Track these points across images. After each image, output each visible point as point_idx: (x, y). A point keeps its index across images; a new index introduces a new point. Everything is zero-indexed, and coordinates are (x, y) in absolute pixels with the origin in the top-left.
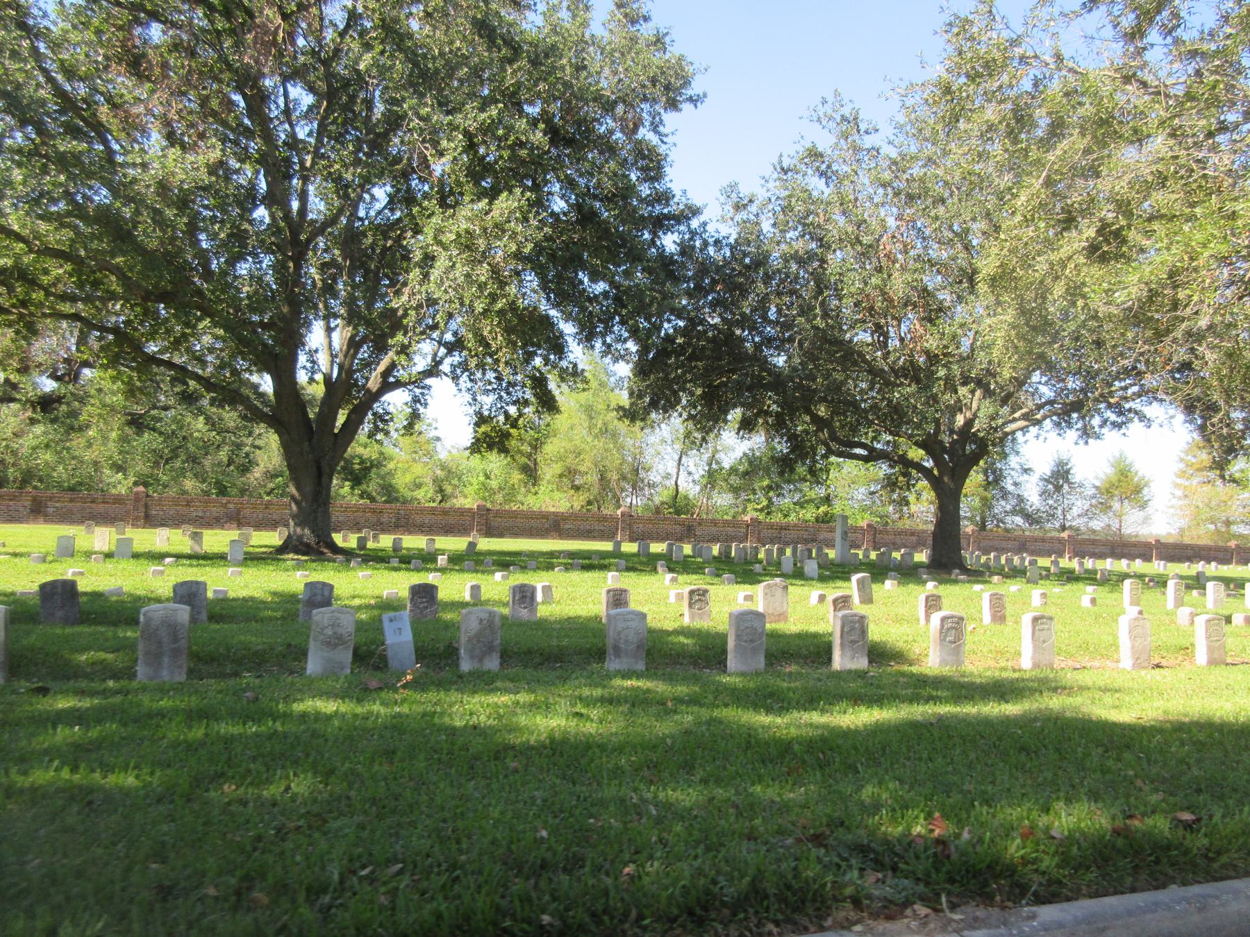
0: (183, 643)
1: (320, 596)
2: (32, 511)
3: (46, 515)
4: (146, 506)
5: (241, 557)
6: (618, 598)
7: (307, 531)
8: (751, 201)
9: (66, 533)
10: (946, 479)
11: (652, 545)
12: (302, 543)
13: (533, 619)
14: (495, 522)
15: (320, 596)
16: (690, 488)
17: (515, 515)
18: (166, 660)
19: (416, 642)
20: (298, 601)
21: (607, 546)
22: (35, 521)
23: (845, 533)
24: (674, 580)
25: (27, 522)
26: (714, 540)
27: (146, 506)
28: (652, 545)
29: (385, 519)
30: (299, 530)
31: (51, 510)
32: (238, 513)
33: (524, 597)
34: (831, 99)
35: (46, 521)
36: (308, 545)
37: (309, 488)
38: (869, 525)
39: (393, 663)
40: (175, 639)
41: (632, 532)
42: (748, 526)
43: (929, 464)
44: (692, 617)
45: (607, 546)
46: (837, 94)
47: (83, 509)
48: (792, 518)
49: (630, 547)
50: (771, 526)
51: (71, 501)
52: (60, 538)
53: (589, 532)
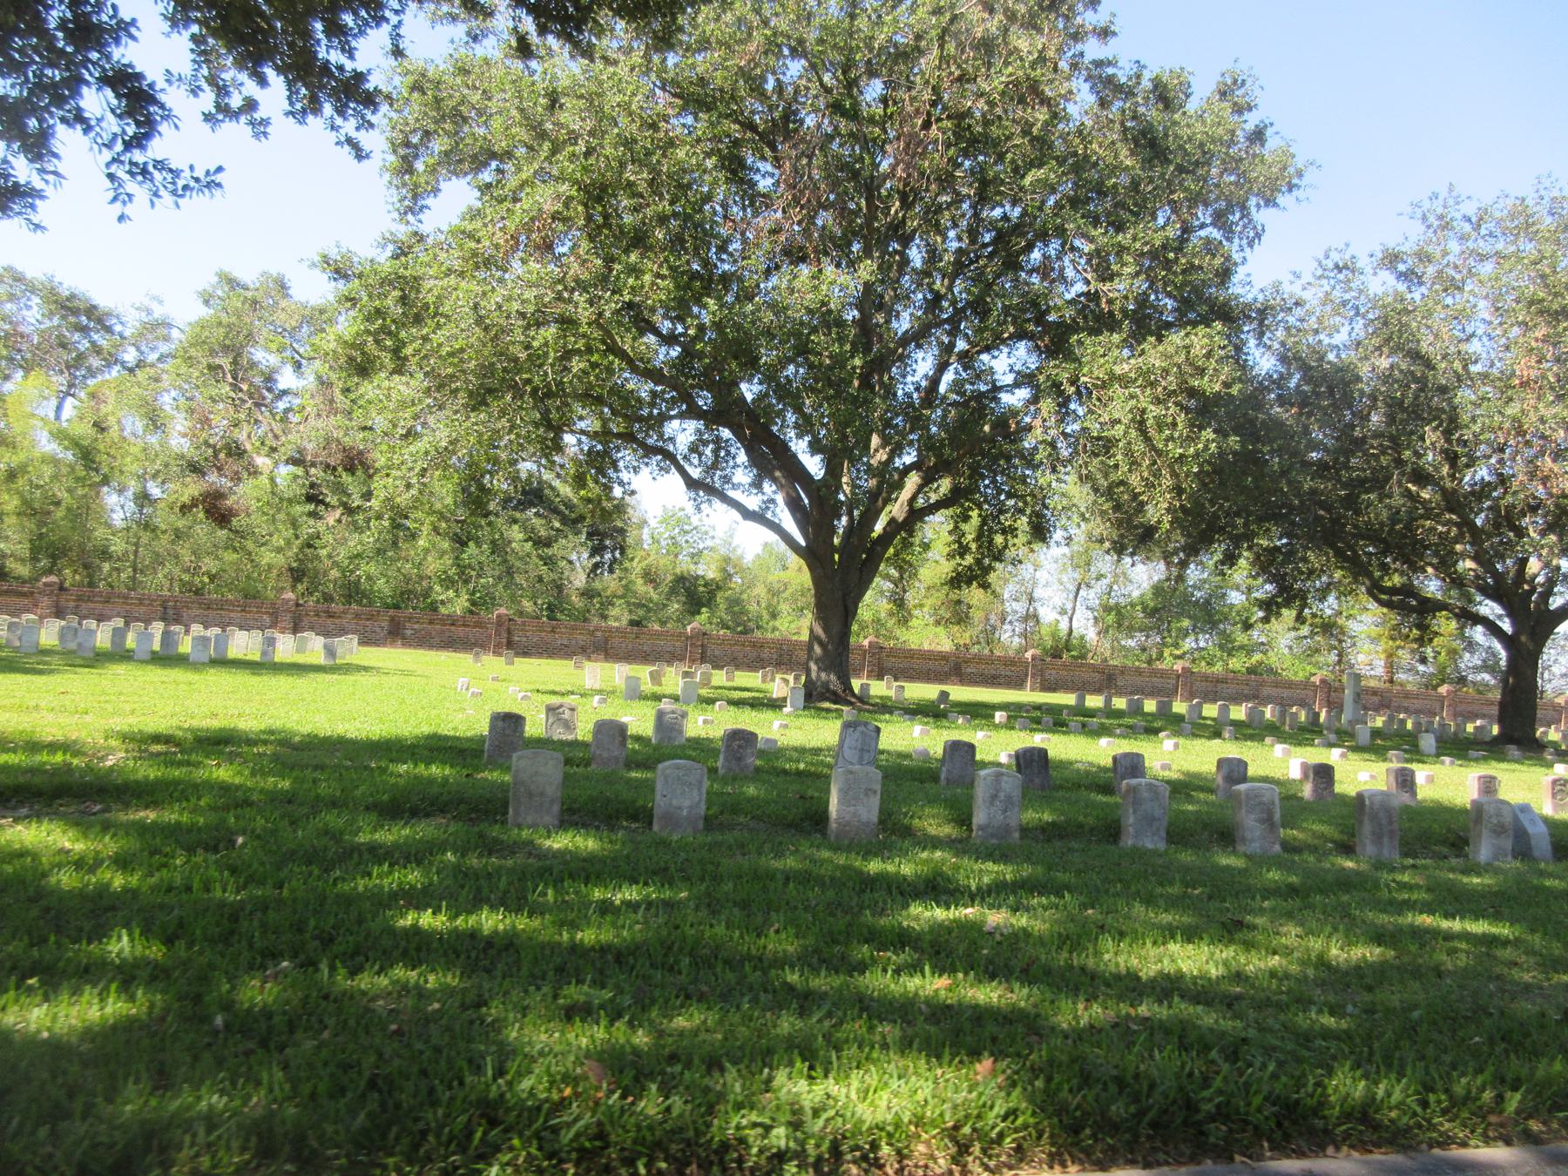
0: (1396, 826)
1: (1131, 765)
2: (390, 633)
3: (404, 638)
4: (509, 632)
5: (148, 657)
6: (1488, 785)
7: (833, 677)
8: (1297, 304)
9: (632, 674)
10: (1523, 638)
11: (1088, 697)
12: (828, 690)
13: (1413, 804)
14: (890, 662)
15: (1131, 765)
16: (1085, 627)
17: (990, 660)
18: (1386, 839)
19: (1552, 835)
20: (714, 752)
21: (1068, 699)
22: (393, 644)
23: (1358, 696)
24: (1176, 746)
25: (384, 645)
26: (1152, 694)
27: (509, 632)
28: (1088, 697)
29: (765, 654)
30: (823, 675)
31: (409, 632)
32: (606, 641)
33: (1405, 781)
34: (1443, 193)
35: (403, 645)
36: (835, 693)
37: (836, 629)
38: (1322, 681)
39: (1536, 853)
40: (1391, 823)
41: (1043, 680)
42: (1178, 676)
43: (1506, 626)
44: (1555, 808)
45: (1068, 699)
46: (1451, 188)
47: (443, 632)
48: (1218, 668)
49: (1239, 712)
50: (1206, 678)
51: (431, 622)
52: (628, 678)
53: (994, 677)
